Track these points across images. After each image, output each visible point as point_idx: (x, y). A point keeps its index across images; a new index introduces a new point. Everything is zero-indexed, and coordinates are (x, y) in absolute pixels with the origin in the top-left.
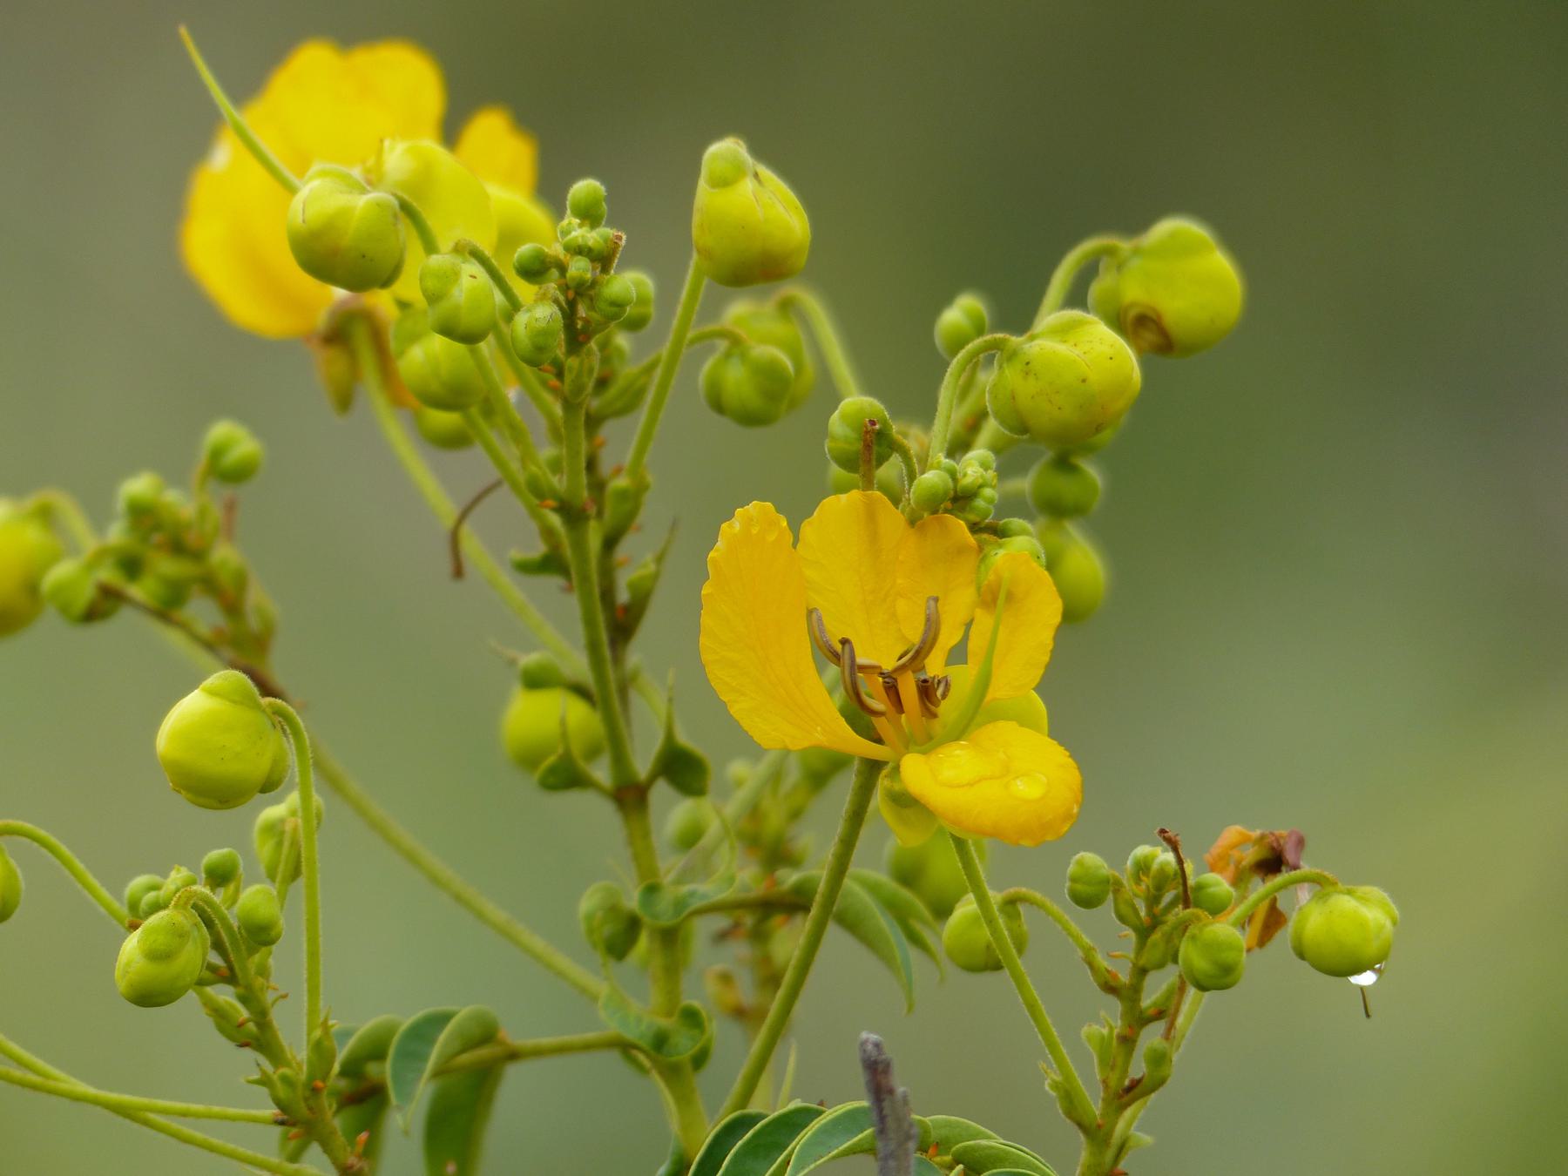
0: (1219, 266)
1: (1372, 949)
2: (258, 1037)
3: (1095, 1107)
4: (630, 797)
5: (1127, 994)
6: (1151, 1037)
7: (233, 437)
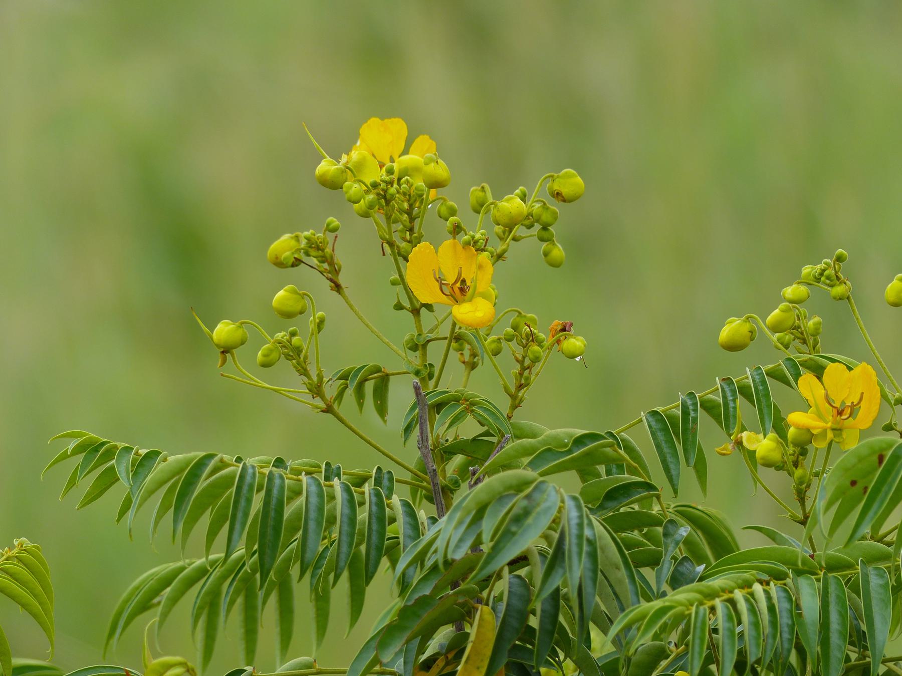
0: (579, 180)
1: (578, 352)
2: (304, 372)
3: (513, 390)
4: (416, 312)
5: (521, 362)
6: (526, 373)
7: (334, 221)
